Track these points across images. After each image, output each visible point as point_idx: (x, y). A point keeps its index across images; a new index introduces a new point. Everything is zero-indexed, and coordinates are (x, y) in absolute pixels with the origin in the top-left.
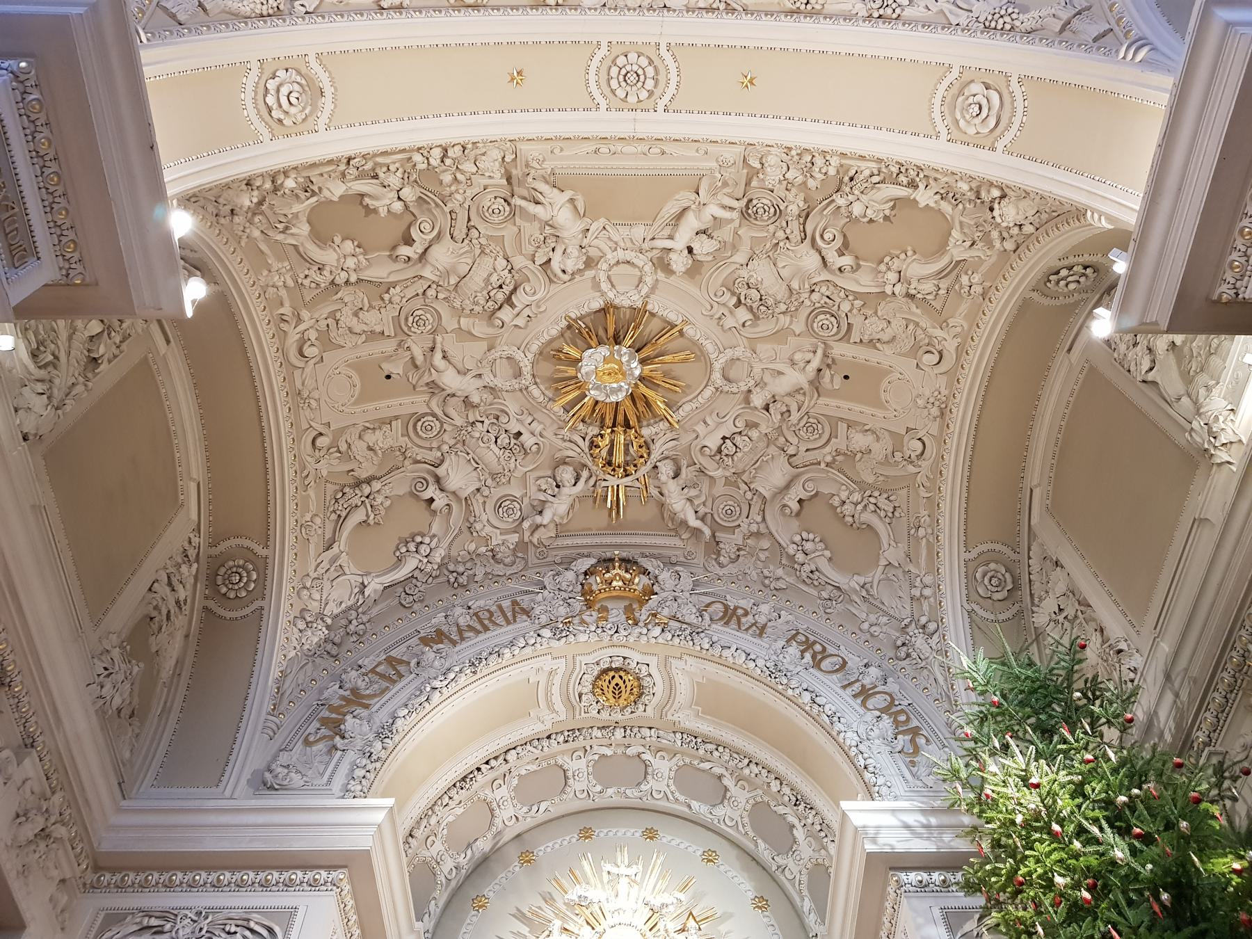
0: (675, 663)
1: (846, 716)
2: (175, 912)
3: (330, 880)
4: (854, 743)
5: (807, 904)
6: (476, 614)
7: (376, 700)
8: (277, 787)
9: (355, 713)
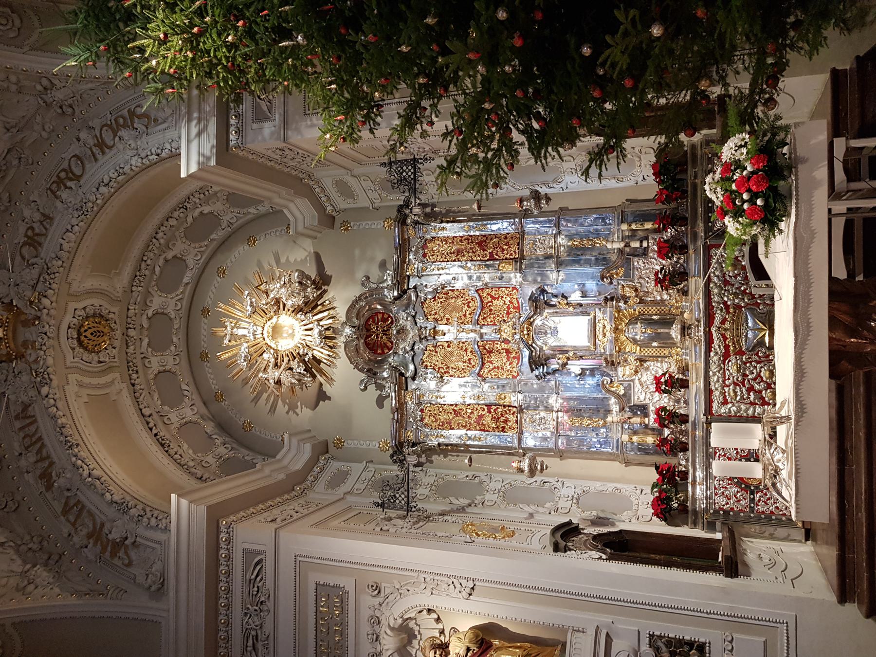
0: (75, 287)
1: (119, 162)
2: (244, 630)
3: (226, 530)
4: (140, 160)
5: (252, 210)
6: (27, 448)
7: (97, 517)
8: (162, 580)
9: (108, 533)
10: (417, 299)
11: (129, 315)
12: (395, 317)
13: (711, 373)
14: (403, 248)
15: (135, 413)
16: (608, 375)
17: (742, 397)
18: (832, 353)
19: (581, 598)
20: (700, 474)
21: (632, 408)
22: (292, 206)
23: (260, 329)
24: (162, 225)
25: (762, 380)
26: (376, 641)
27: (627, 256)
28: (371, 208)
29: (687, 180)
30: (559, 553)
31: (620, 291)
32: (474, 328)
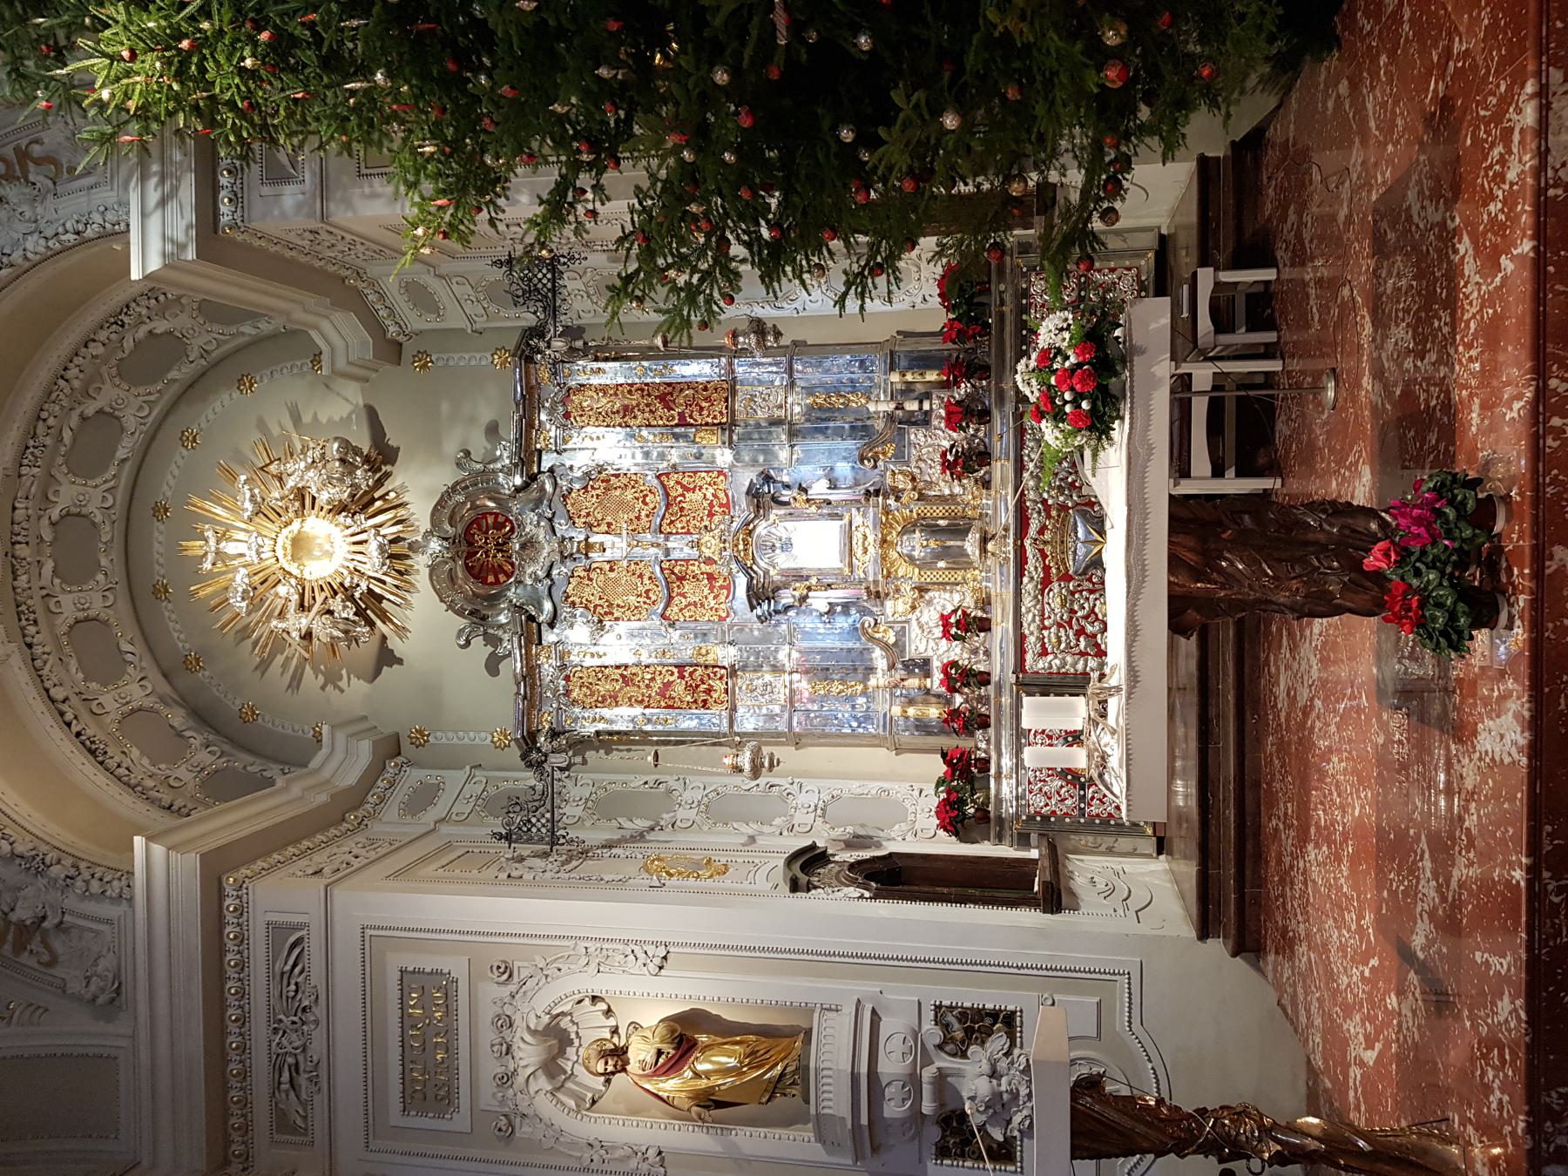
4: (42, 242)
5: (247, 329)
10: (555, 489)
11: (17, 519)
12: (517, 519)
13: (1023, 609)
14: (529, 402)
15: (37, 697)
16: (871, 613)
17: (1068, 644)
18: (1172, 598)
19: (833, 959)
20: (1007, 762)
21: (906, 665)
22: (326, 326)
23: (268, 542)
24: (76, 355)
25: (1097, 619)
26: (507, 1054)
27: (901, 422)
28: (469, 331)
29: (990, 306)
30: (799, 894)
31: (889, 481)
32: (654, 540)
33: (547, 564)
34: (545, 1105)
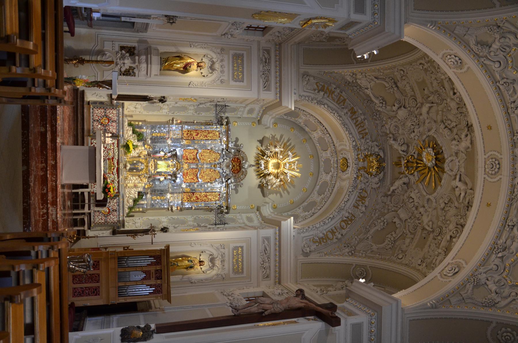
33: (224, 162)
34: (214, 56)
